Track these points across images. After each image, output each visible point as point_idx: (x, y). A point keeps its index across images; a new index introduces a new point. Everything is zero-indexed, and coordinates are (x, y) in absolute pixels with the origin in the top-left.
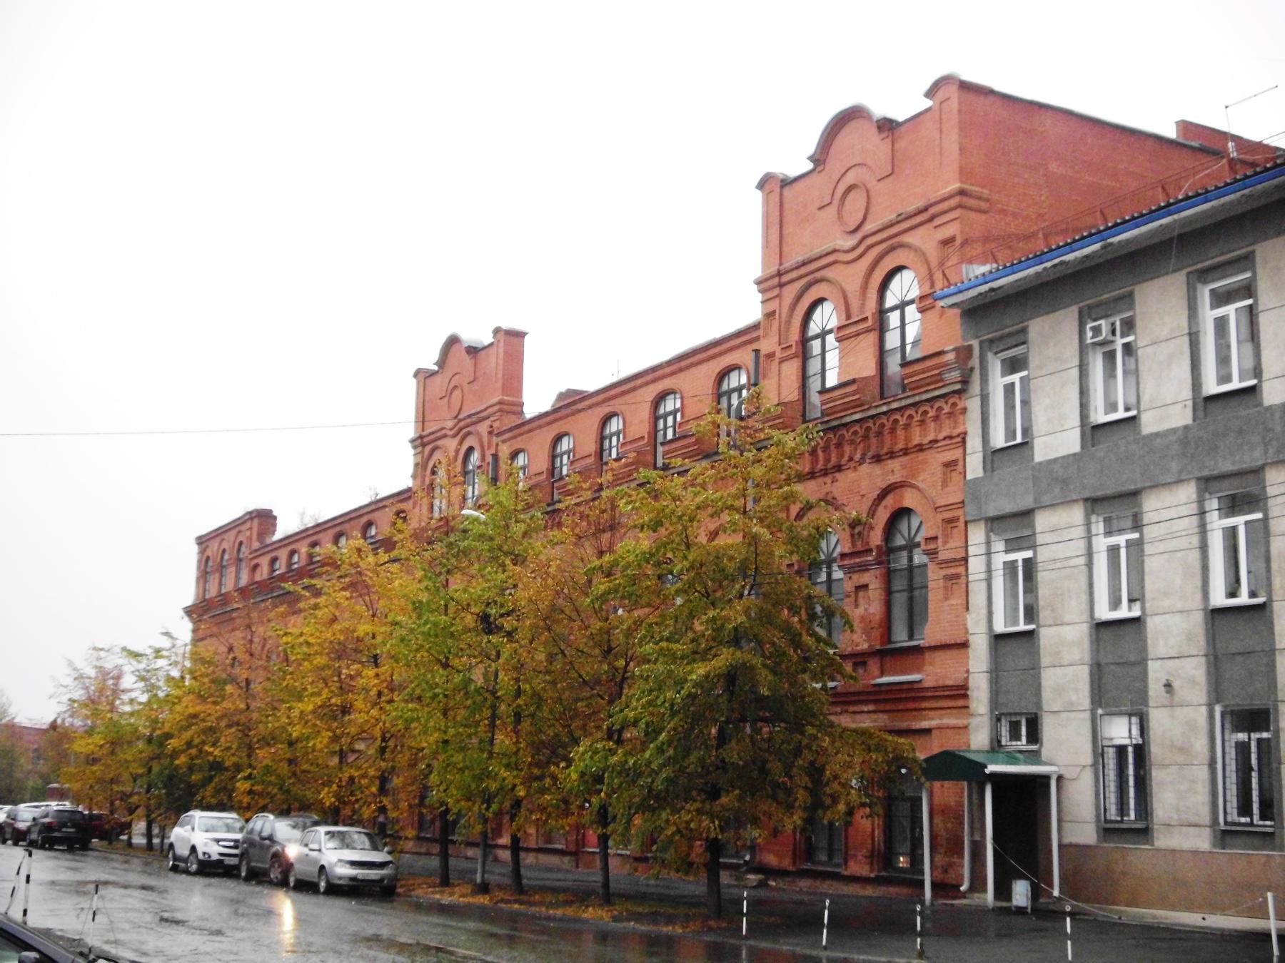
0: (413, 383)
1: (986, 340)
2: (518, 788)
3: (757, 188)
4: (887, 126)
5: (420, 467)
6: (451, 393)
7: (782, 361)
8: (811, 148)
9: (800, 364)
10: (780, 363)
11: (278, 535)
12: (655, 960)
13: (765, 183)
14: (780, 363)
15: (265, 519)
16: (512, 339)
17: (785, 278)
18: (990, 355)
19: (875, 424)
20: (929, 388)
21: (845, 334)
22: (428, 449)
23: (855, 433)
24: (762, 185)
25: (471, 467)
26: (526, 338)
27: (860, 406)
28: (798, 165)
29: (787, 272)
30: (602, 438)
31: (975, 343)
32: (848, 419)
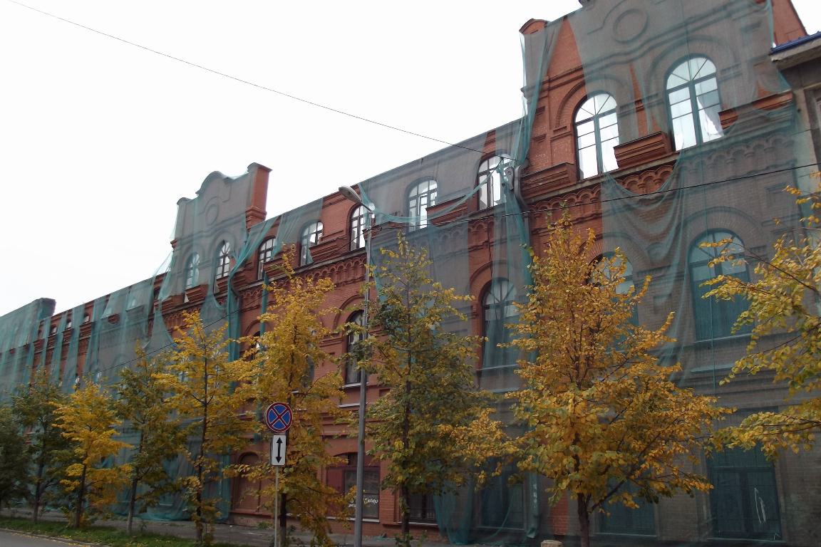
0: (175, 208)
1: (810, 90)
2: (572, 465)
3: (520, 30)
4: (228, 180)
5: (176, 261)
6: (209, 210)
7: (553, 140)
8: (198, 188)
9: (573, 140)
10: (552, 141)
11: (54, 314)
12: (139, 545)
13: (529, 28)
14: (552, 141)
15: (48, 304)
16: (260, 173)
17: (553, 84)
18: (814, 100)
19: (345, 265)
20: (544, 192)
21: (202, 266)
22: (185, 248)
23: (586, 196)
24: (524, 30)
25: (192, 266)
26: (270, 174)
27: (661, 154)
28: (192, 196)
29: (554, 80)
30: (351, 220)
31: (800, 93)
32: (562, 192)
